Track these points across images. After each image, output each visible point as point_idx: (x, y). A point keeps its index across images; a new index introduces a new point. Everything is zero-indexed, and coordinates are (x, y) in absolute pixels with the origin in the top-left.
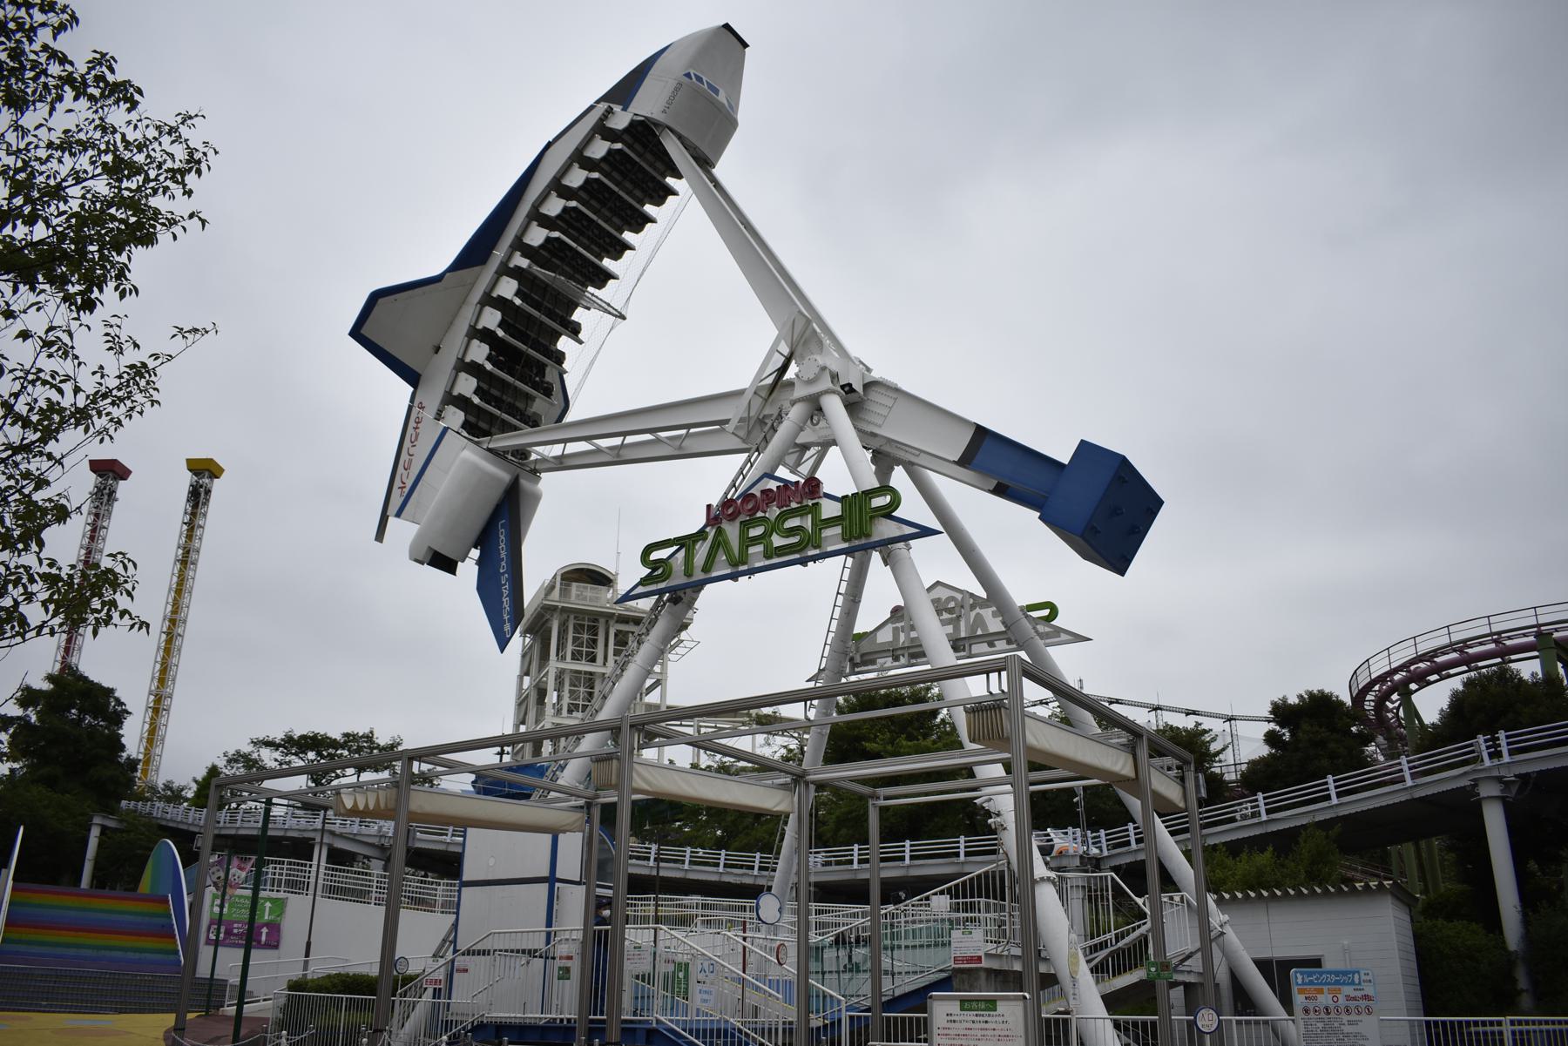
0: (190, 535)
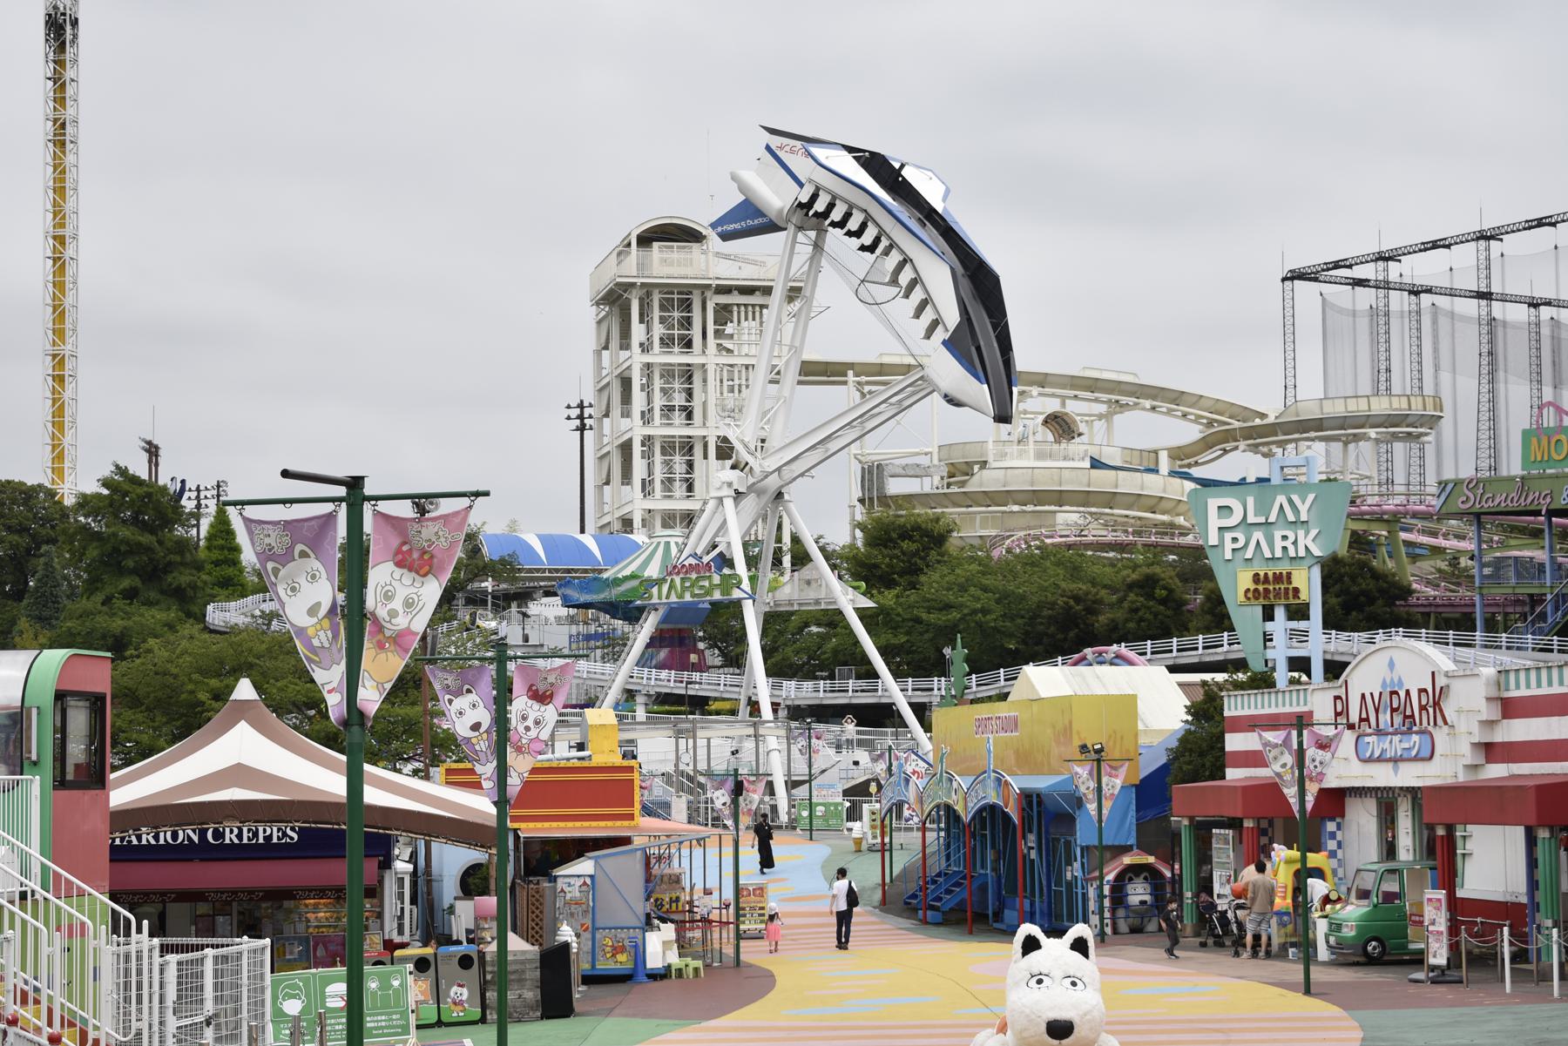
0: (60, 100)
